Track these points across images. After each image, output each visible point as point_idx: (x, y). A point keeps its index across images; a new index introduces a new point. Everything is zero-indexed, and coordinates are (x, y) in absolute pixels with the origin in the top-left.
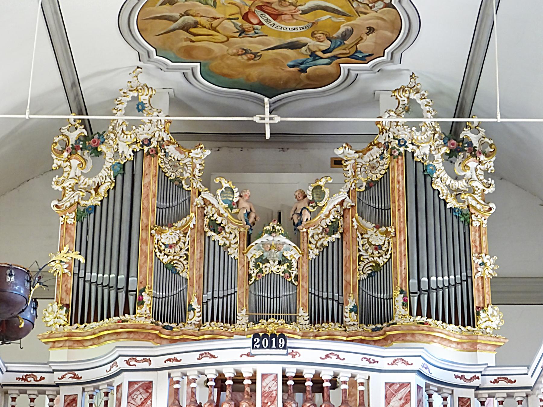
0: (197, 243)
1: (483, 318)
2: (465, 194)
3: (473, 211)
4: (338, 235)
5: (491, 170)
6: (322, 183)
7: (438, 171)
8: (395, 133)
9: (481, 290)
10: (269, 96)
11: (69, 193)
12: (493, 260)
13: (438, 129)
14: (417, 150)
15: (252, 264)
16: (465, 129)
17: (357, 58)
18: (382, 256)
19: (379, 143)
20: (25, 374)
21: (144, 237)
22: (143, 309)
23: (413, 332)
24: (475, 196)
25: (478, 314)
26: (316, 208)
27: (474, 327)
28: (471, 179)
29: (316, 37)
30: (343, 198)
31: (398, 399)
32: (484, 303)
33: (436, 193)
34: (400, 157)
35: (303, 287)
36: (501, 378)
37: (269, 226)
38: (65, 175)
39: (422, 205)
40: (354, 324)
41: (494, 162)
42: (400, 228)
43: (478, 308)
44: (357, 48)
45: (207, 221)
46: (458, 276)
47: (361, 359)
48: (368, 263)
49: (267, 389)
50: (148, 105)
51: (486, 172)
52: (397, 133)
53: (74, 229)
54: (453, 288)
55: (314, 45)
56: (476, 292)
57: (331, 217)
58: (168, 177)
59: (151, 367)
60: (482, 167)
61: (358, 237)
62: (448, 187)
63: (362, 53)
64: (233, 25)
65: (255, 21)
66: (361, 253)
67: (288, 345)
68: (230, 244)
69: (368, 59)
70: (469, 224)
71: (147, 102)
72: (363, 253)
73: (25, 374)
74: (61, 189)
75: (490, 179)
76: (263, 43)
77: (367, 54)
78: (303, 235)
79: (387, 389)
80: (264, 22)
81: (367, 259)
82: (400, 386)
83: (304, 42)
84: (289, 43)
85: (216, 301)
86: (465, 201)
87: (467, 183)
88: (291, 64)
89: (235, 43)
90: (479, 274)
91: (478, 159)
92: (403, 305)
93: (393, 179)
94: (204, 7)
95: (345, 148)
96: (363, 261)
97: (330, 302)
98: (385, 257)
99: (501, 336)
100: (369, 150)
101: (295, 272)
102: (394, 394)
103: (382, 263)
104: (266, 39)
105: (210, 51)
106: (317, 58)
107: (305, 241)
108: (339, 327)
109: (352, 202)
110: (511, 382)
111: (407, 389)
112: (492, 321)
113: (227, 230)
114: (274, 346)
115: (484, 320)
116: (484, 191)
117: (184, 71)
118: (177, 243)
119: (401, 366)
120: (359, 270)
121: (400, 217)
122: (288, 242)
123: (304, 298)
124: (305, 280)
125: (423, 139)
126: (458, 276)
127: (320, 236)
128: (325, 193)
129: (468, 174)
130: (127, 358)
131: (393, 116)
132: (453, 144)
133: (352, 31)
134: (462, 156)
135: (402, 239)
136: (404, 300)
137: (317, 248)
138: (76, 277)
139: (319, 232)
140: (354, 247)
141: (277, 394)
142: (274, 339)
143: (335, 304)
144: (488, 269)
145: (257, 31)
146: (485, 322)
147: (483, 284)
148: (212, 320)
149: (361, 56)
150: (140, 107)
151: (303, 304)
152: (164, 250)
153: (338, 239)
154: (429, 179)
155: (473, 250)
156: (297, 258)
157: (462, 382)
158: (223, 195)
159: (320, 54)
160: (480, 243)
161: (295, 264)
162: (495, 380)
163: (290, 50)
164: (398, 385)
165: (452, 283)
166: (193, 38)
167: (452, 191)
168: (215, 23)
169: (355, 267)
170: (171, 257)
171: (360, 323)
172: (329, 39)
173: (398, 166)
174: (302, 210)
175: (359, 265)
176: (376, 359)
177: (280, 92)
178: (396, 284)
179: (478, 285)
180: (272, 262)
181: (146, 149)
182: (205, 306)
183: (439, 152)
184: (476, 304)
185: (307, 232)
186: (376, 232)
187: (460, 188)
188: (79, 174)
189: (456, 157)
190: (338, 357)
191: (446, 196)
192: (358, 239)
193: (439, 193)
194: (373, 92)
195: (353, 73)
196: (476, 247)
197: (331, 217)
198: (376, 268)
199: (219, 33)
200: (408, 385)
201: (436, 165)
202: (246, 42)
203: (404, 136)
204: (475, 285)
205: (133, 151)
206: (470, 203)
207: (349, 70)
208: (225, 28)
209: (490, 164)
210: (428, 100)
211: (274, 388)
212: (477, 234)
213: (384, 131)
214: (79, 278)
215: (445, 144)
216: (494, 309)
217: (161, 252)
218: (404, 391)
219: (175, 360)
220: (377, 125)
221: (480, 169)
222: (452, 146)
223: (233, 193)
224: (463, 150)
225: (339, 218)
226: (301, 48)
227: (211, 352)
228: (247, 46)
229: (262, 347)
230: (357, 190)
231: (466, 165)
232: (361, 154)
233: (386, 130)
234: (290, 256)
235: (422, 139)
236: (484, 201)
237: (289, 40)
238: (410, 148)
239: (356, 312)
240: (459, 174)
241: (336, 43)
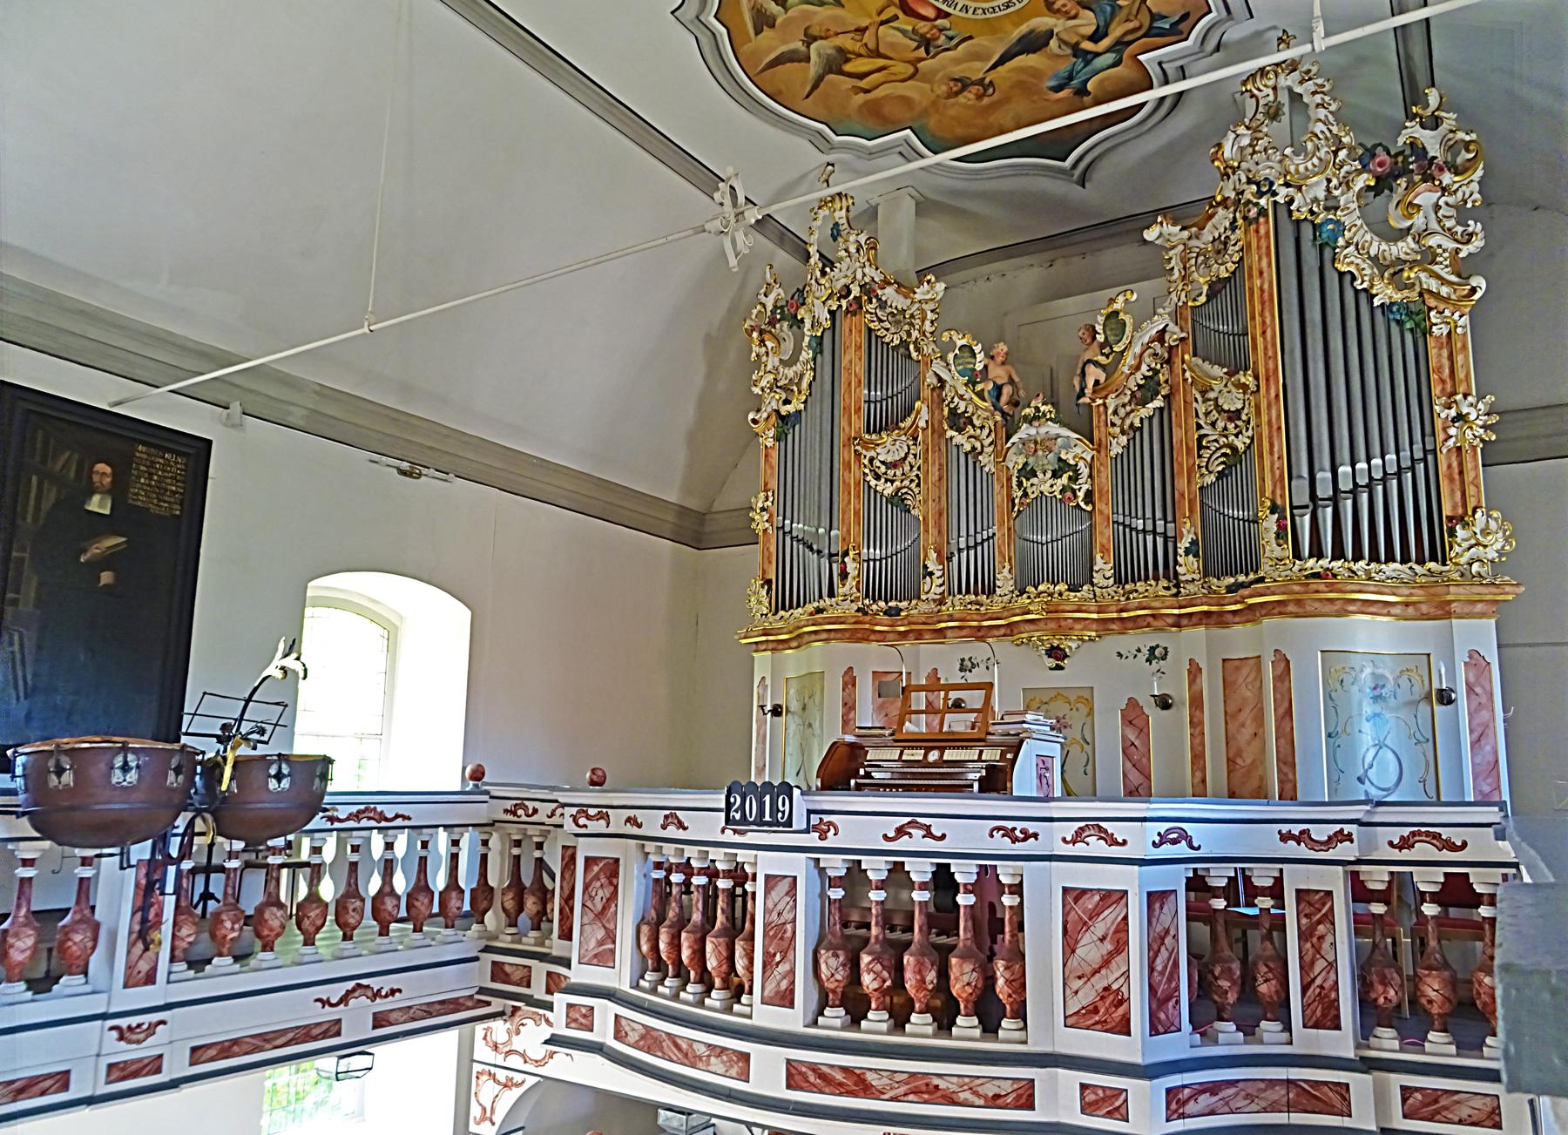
0: (933, 452)
1: (1464, 540)
2: (1411, 269)
3: (1432, 302)
4: (1158, 403)
5: (1474, 201)
6: (1118, 306)
7: (1350, 230)
8: (1250, 171)
9: (1457, 477)
10: (1058, 155)
11: (767, 398)
12: (1485, 404)
13: (1346, 140)
14: (1298, 197)
16: (1407, 124)
17: (1162, 33)
18: (1241, 432)
19: (1225, 199)
20: (515, 802)
21: (847, 458)
22: (848, 586)
23: (1298, 597)
24: (1436, 268)
25: (1452, 533)
26: (1111, 357)
27: (1444, 564)
29: (1058, 11)
30: (1161, 327)
31: (1095, 938)
32: (1465, 506)
33: (1348, 278)
35: (1101, 512)
36: (1420, 833)
37: (1029, 406)
39: (1314, 313)
40: (1193, 580)
41: (1479, 183)
42: (1267, 370)
43: (1450, 519)
44: (1150, 10)
46: (1405, 454)
47: (988, 832)
48: (1218, 449)
49: (774, 916)
50: (846, 225)
51: (1460, 208)
52: (1253, 169)
53: (774, 454)
54: (1395, 482)
55: (1066, 30)
56: (1446, 482)
58: (888, 344)
59: (610, 830)
60: (1451, 200)
61: (1196, 400)
62: (1375, 260)
63: (1166, 17)
64: (900, 35)
65: (931, 13)
66: (1202, 432)
68: (982, 446)
69: (1183, 26)
70: (1427, 332)
71: (844, 221)
73: (515, 802)
75: (1471, 222)
76: (977, 56)
77: (1177, 18)
78: (1098, 412)
79: (1068, 907)
81: (1216, 441)
82: (1101, 899)
83: (1044, 28)
84: (1020, 39)
86: (1413, 284)
87: (1418, 242)
88: (1052, 83)
89: (933, 72)
90: (1451, 443)
91: (1437, 183)
92: (1278, 536)
93: (1250, 268)
95: (1161, 223)
96: (1208, 448)
98: (1246, 434)
99: (1507, 578)
100: (1211, 217)
101: (1085, 487)
102: (1085, 923)
103: (1241, 447)
104: (973, 45)
106: (1089, 57)
107: (1102, 424)
108: (1165, 588)
109: (1182, 331)
110: (1452, 847)
111: (1117, 911)
112: (1485, 546)
113: (977, 423)
114: (767, 818)
115: (1465, 545)
116: (1457, 253)
117: (898, 149)
118: (905, 458)
119: (1097, 847)
120: (1199, 467)
121: (1266, 348)
122: (1065, 432)
123: (1104, 535)
124: (1104, 498)
125: (1310, 167)
127: (1128, 408)
128: (1125, 324)
129: (1418, 220)
131: (1244, 135)
134: (1404, 185)
135: (1273, 394)
136: (1279, 526)
137: (1123, 432)
138: (781, 532)
139: (1126, 400)
140: (1190, 421)
141: (794, 933)
142: (767, 798)
144: (1471, 428)
145: (950, 33)
146: (1469, 549)
147: (1461, 464)
148: (960, 592)
149: (1167, 26)
151: (1102, 546)
152: (885, 473)
153: (1161, 409)
154: (1328, 253)
155: (1436, 390)
156: (1089, 459)
157: (1303, 851)
158: (958, 362)
162: (1402, 838)
163: (1031, 56)
164: (1097, 898)
166: (864, 84)
167: (1382, 268)
169: (1191, 462)
170: (898, 484)
171: (1205, 577)
173: (1259, 240)
174: (1085, 365)
175: (1200, 456)
176: (1031, 827)
177: (1072, 146)
178: (1263, 494)
179: (1449, 466)
180: (1040, 475)
181: (844, 303)
183: (1349, 188)
184: (1446, 511)
185: (1104, 405)
186: (1226, 386)
187: (1403, 256)
189: (1391, 190)
190: (929, 833)
191: (1371, 280)
192: (1195, 404)
193: (1354, 278)
196: (1443, 381)
197: (1144, 368)
198: (1234, 457)
199: (891, 59)
200: (1122, 898)
201: (1343, 219)
202: (945, 63)
203: (1268, 171)
204: (1443, 468)
205: (829, 311)
206: (1425, 287)
209: (1470, 188)
210: (1320, 81)
211: (787, 916)
212: (1445, 353)
213: (1230, 171)
214: (784, 533)
215: (1364, 167)
216: (1489, 516)
218: (1110, 917)
220: (1213, 161)
221: (1447, 204)
222: (1379, 170)
223: (974, 355)
224: (1406, 172)
225: (1158, 367)
226: (1048, 44)
230: (1190, 304)
231: (1410, 203)
232: (1194, 230)
233: (1232, 167)
234: (1074, 457)
235: (1306, 169)
236: (1459, 276)
237: (1017, 33)
238: (1282, 194)
239: (1196, 555)
240: (1400, 226)
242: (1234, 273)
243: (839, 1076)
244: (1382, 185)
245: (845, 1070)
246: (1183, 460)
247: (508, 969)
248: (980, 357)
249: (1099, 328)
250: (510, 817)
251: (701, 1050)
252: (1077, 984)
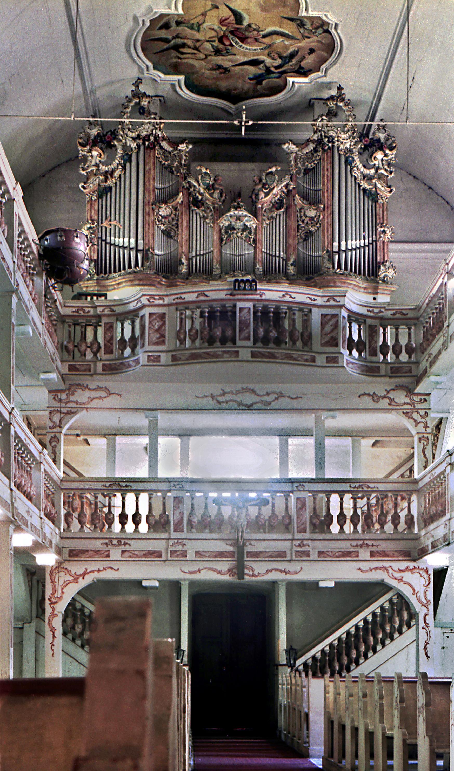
15: (223, 231)
25: (380, 267)
34: (329, 151)
38: (88, 163)
45: (191, 199)
57: (279, 196)
62: (362, 173)
65: (227, 43)
67: (258, 287)
74: (85, 174)
76: (231, 61)
80: (234, 44)
85: (198, 258)
89: (211, 61)
93: (324, 167)
94: (191, 32)
97: (277, 259)
105: (193, 66)
119: (332, 303)
122: (249, 215)
126: (366, 241)
130: (148, 297)
132: (366, 141)
133: (297, 52)
137: (268, 219)
143: (281, 260)
150: (141, 111)
160: (383, 217)
161: (253, 231)
168: (198, 44)
172: (280, 57)
176: (316, 298)
182: (191, 261)
188: (98, 162)
190: (291, 297)
194: (308, 101)
195: (296, 85)
196: (380, 219)
207: (293, 83)
208: (204, 48)
211: (248, 318)
212: (381, 209)
219: (181, 298)
227: (206, 293)
228: (220, 63)
229: (239, 289)
241: (285, 61)
242: (314, 168)
243: (267, 354)
244: (366, 148)
245: (269, 352)
246: (293, 233)
247: (77, 366)
249: (263, 177)
250: (76, 314)
251: (220, 353)
252: (324, 336)
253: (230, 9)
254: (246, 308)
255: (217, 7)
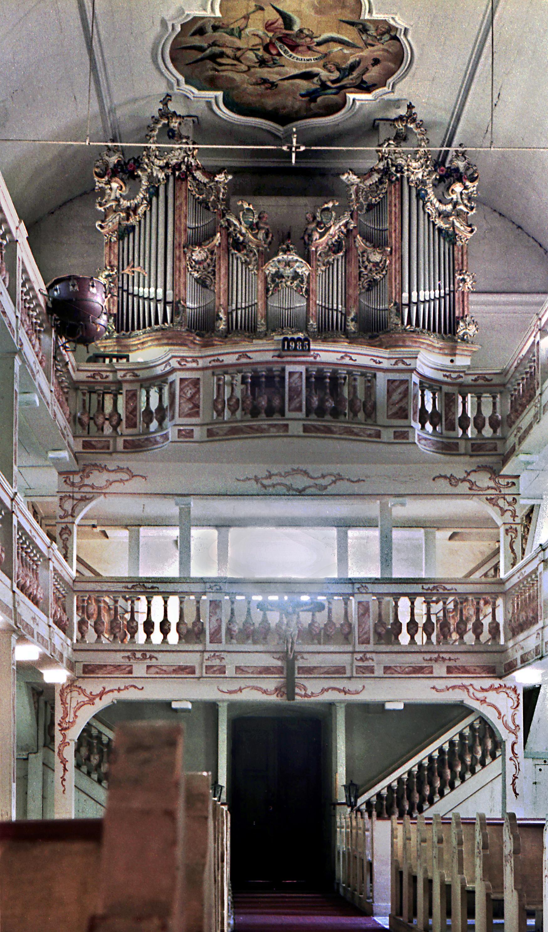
15: (269, 279)
25: (458, 323)
28: (455, 204)
34: (397, 182)
38: (107, 197)
45: (231, 241)
57: (336, 237)
62: (437, 209)
65: (274, 52)
67: (312, 347)
72: (363, 269)
74: (103, 210)
80: (282, 53)
85: (239, 312)
89: (255, 73)
93: (391, 202)
94: (230, 38)
97: (335, 313)
105: (233, 80)
119: (401, 366)
122: (300, 259)
126: (442, 291)
130: (179, 359)
132: (442, 171)
133: (359, 63)
137: (324, 265)
143: (339, 315)
150: (171, 134)
159: (329, 84)
160: (462, 262)
161: (305, 280)
165: (437, 296)
168: (239, 53)
172: (338, 69)
176: (381, 360)
182: (230, 316)
190: (351, 359)
196: (458, 264)
207: (354, 100)
208: (247, 58)
211: (299, 384)
212: (460, 253)
217: (192, 268)
219: (218, 360)
227: (249, 354)
228: (266, 76)
229: (288, 349)
243: (322, 428)
244: (441, 179)
245: (324, 426)
246: (353, 282)
247: (93, 443)
248: (256, 216)
249: (318, 214)
250: (92, 380)
251: (266, 427)
252: (391, 407)
253: (278, 11)
254: (297, 372)
255: (262, 9)
